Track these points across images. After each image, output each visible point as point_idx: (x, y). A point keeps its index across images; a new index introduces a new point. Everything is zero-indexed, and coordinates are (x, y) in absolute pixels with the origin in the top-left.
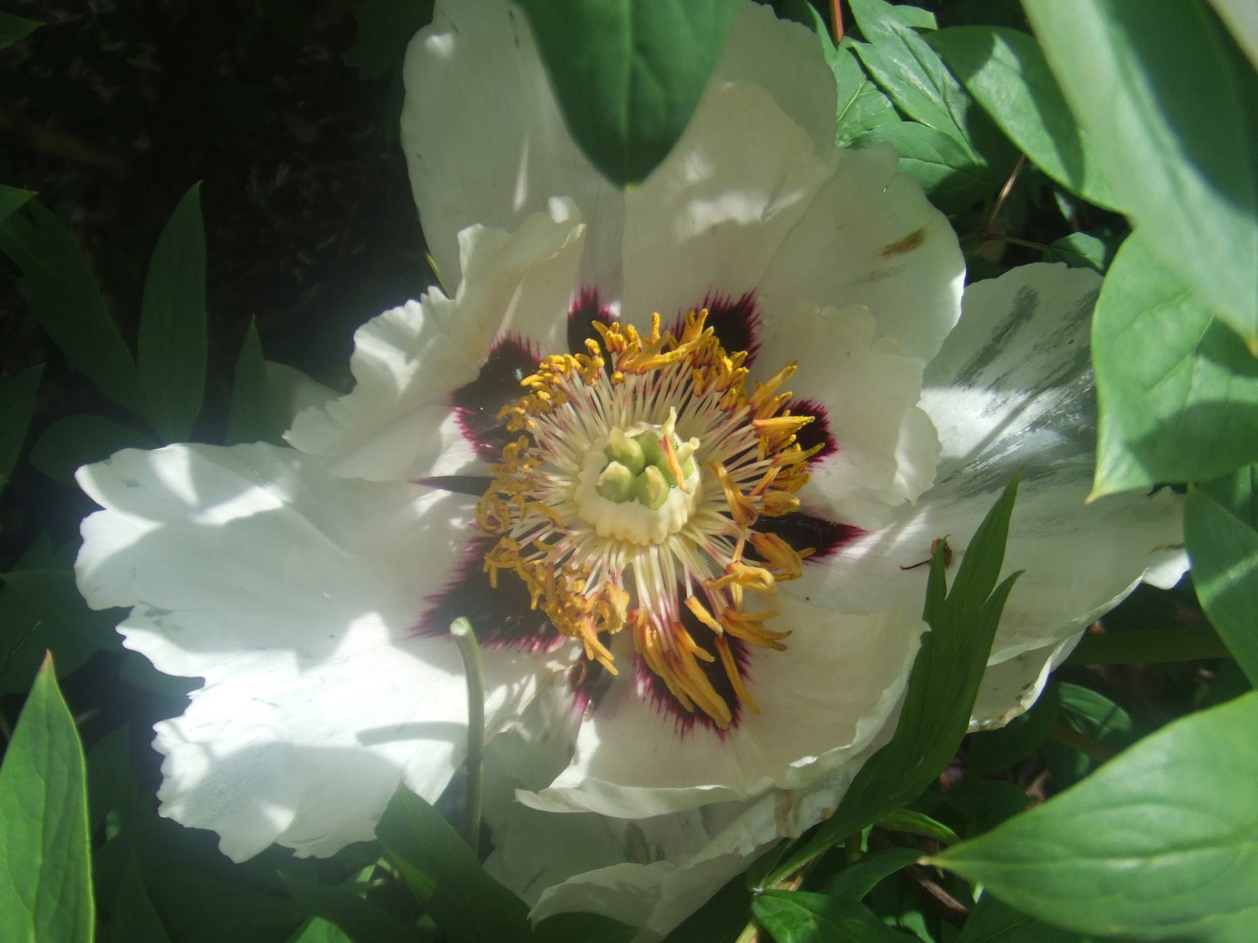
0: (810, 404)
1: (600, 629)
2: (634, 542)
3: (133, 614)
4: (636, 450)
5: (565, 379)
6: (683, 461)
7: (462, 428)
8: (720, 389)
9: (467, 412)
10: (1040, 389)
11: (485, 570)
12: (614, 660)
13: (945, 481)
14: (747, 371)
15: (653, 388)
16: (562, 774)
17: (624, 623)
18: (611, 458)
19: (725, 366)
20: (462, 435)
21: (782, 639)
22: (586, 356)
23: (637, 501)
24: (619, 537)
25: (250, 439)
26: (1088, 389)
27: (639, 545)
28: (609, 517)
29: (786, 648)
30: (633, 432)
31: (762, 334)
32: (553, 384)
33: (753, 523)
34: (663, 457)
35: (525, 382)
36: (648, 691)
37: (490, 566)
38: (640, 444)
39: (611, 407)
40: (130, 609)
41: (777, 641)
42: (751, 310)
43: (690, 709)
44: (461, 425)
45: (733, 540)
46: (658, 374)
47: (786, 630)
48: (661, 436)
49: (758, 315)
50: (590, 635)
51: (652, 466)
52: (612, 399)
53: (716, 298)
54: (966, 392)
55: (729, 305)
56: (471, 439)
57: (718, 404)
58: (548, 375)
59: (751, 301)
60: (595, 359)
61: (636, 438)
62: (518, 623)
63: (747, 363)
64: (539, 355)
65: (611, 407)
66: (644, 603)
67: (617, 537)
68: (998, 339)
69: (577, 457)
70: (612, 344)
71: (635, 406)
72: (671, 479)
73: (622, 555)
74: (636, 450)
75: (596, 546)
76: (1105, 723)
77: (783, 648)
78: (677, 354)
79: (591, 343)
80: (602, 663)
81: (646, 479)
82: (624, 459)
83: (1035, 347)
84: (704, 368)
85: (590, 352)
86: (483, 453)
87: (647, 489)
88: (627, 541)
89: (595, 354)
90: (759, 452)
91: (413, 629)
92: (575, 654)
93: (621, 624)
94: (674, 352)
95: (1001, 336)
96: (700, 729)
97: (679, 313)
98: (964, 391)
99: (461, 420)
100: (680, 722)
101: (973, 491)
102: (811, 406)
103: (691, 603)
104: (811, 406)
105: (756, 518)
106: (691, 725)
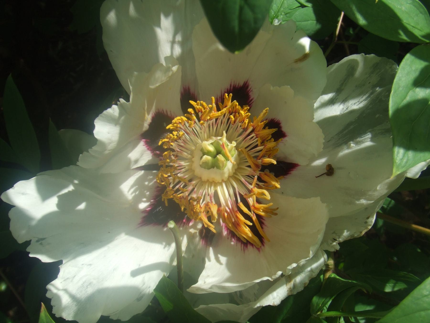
0: (274, 120)
1: (208, 215)
2: (217, 182)
3: (32, 242)
4: (211, 149)
5: (182, 126)
6: (230, 151)
7: (146, 147)
8: (241, 121)
9: (147, 140)
10: (360, 102)
11: (163, 200)
12: (215, 227)
13: (329, 141)
14: (250, 114)
15: (216, 124)
16: (203, 272)
17: (217, 219)
18: (204, 154)
19: (241, 114)
20: (147, 150)
21: (275, 211)
22: (189, 115)
23: (215, 168)
24: (211, 181)
25: (68, 165)
26: (378, 101)
27: (218, 182)
28: (206, 174)
29: (277, 214)
30: (211, 141)
31: (254, 95)
32: (178, 127)
33: (260, 169)
34: (223, 151)
35: (168, 127)
36: (229, 235)
37: (164, 198)
38: (214, 146)
39: (201, 133)
40: (30, 241)
41: (273, 212)
42: (248, 87)
43: (245, 241)
44: (146, 146)
45: (252, 177)
46: (216, 120)
47: (277, 207)
48: (221, 143)
49: (251, 88)
50: (205, 220)
51: (219, 155)
52: (201, 130)
53: (234, 84)
54: (332, 106)
55: (239, 86)
56: (150, 150)
57: (241, 126)
58: (175, 125)
59: (247, 84)
60: (192, 115)
61: (212, 144)
62: (178, 216)
63: (249, 111)
64: (171, 115)
65: (201, 133)
66: (223, 205)
67: (210, 181)
68: (342, 85)
69: (191, 153)
70: (198, 110)
71: (210, 130)
72: (227, 159)
73: (212, 188)
74: (211, 149)
75: (202, 185)
76: (388, 206)
77: (276, 214)
78: (223, 112)
79: (190, 110)
80: (211, 229)
81: (218, 160)
82: (208, 153)
83: (356, 86)
84: (233, 114)
85: (190, 113)
86: (155, 155)
87: (219, 163)
88: (214, 181)
89: (192, 114)
90: (259, 143)
91: (139, 224)
92: (200, 226)
93: (216, 219)
94: (222, 111)
95: (342, 84)
96: (250, 247)
97: (221, 91)
98: (331, 106)
99: (146, 144)
100: (243, 246)
101: (339, 144)
102: (275, 120)
103: (240, 205)
104: (275, 120)
105: (260, 168)
106: (247, 246)
